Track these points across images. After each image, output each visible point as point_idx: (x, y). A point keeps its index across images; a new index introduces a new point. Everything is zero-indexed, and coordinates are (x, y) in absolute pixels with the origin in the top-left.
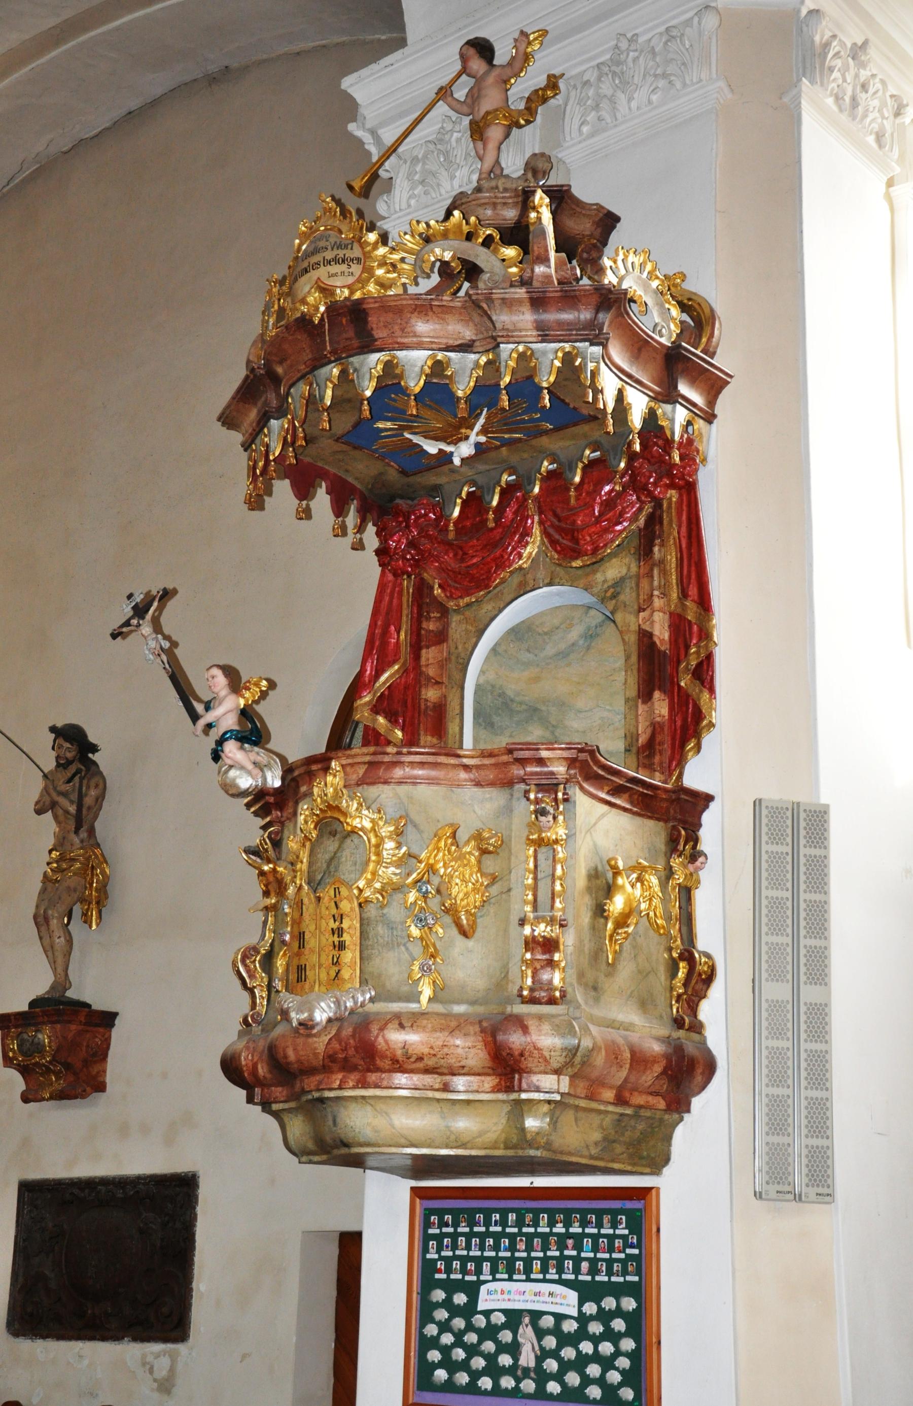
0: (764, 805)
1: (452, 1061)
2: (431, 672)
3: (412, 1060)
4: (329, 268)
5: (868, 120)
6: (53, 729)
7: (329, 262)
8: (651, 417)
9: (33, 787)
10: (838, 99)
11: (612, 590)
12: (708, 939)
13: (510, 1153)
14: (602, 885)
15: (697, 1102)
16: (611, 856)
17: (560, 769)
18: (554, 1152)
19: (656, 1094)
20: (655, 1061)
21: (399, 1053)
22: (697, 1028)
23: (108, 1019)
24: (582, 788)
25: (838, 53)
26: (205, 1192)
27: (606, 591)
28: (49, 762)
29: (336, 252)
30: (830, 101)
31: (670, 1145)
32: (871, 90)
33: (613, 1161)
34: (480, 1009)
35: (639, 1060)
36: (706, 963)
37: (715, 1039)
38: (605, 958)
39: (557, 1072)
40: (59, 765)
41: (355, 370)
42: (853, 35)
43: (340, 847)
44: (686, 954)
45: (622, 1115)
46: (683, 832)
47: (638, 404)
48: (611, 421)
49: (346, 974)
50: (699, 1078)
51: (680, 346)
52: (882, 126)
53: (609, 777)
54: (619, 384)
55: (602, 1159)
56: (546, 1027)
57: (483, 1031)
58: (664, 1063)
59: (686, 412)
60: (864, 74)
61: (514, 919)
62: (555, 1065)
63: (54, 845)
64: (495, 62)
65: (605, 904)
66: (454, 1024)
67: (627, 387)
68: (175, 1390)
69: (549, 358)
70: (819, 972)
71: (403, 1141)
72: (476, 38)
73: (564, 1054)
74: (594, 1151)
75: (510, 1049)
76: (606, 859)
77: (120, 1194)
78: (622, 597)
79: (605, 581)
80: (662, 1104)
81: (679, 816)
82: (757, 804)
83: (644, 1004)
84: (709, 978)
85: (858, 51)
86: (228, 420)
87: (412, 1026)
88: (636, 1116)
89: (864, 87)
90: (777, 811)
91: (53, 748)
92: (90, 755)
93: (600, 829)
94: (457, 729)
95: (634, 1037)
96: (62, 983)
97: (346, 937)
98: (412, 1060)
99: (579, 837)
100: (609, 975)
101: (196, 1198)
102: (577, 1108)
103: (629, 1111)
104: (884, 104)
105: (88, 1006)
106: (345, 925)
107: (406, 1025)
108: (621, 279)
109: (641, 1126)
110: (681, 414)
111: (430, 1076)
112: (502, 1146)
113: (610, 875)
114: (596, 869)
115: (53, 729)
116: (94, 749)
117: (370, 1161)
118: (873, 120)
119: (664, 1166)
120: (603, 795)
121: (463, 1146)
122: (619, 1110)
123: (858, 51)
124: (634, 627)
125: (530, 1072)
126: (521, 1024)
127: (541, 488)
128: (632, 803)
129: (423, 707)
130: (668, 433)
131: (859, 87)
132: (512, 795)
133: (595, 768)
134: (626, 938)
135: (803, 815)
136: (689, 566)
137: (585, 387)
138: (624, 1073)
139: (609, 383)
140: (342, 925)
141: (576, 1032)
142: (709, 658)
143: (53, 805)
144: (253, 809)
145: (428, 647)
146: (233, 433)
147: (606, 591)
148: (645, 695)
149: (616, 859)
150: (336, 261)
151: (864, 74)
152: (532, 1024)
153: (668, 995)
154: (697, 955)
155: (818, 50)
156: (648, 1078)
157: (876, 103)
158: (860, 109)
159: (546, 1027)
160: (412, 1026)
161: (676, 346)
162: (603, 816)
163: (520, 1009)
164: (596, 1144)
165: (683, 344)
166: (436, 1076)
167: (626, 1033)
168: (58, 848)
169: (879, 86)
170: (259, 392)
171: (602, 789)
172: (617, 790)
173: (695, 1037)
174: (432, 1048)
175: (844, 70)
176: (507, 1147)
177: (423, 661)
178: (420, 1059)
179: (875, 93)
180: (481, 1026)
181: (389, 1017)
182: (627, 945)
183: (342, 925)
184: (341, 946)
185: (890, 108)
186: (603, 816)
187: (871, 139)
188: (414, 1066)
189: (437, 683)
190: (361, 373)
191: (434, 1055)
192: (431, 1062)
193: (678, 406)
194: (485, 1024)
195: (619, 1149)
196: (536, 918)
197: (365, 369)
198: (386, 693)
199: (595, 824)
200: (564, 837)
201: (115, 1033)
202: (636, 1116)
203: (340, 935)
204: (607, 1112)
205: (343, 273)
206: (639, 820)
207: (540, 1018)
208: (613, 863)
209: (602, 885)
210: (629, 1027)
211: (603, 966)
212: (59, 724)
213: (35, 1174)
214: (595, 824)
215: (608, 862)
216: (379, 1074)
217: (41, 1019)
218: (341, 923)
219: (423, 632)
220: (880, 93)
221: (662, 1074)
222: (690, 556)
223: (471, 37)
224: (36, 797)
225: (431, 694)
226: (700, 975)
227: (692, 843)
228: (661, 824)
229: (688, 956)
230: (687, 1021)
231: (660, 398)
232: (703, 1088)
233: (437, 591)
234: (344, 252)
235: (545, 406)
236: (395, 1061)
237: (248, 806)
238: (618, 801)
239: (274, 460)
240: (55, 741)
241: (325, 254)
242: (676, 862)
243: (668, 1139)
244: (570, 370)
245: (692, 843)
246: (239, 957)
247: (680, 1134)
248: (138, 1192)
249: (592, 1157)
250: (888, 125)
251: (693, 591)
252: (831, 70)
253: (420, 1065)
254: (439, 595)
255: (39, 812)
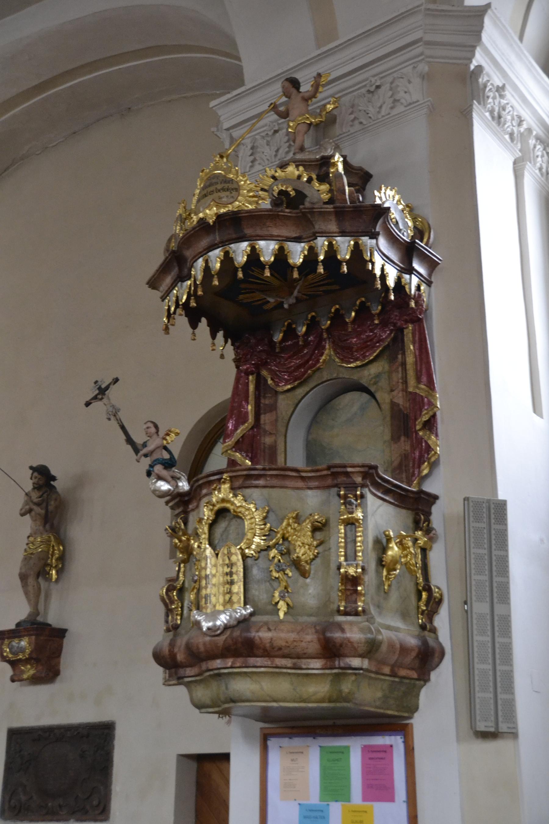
0: (470, 501)
1: (299, 650)
2: (267, 427)
3: (276, 649)
4: (219, 194)
5: (506, 126)
6: (31, 468)
7: (219, 191)
8: (399, 281)
9: (19, 501)
10: (492, 112)
11: (374, 380)
12: (439, 579)
13: (332, 705)
14: (381, 546)
15: (433, 675)
16: (385, 529)
17: (359, 479)
18: (356, 704)
19: (412, 669)
20: (412, 650)
21: (268, 645)
22: (434, 630)
23: (61, 633)
24: (370, 490)
25: (491, 89)
26: (119, 732)
27: (370, 381)
28: (29, 486)
29: (223, 185)
30: (487, 114)
31: (418, 700)
32: (507, 111)
33: (388, 709)
34: (313, 619)
35: (404, 650)
36: (438, 592)
37: (444, 636)
38: (383, 589)
39: (362, 656)
40: (34, 488)
41: (234, 252)
42: (498, 81)
43: (229, 524)
44: (427, 587)
45: (393, 682)
46: (422, 517)
47: (392, 274)
48: (379, 282)
49: (235, 598)
50: (436, 660)
51: (415, 242)
52: (512, 130)
53: (383, 484)
54: (382, 262)
55: (382, 708)
56: (355, 629)
57: (317, 632)
58: (417, 651)
59: (417, 279)
60: (504, 102)
61: (333, 566)
62: (360, 651)
63: (31, 534)
64: (301, 90)
65: (383, 557)
66: (299, 628)
67: (386, 264)
68: (115, 377)
69: (344, 247)
70: (505, 597)
71: (268, 698)
72: (291, 77)
73: (367, 645)
74: (378, 703)
75: (335, 642)
76: (382, 531)
77: (69, 734)
78: (380, 384)
79: (370, 375)
80: (415, 675)
81: (418, 506)
82: (466, 499)
83: (404, 615)
84: (439, 602)
85: (500, 90)
86: (153, 284)
87: (275, 629)
88: (401, 682)
89: (504, 109)
90: (478, 504)
91: (31, 479)
92: (52, 483)
93: (378, 514)
94: (283, 460)
95: (401, 635)
96: (36, 613)
97: (235, 577)
98: (276, 649)
99: (369, 517)
100: (386, 599)
101: (114, 735)
102: (371, 678)
103: (397, 680)
104: (513, 119)
105: (50, 625)
106: (234, 570)
107: (271, 628)
108: (384, 203)
109: (403, 689)
110: (415, 280)
111: (285, 659)
112: (327, 701)
113: (384, 541)
114: (377, 538)
115: (31, 468)
116: (54, 478)
117: (234, 711)
118: (508, 127)
119: (415, 712)
120: (380, 494)
121: (304, 701)
122: (392, 679)
123: (500, 90)
124: (388, 400)
125: (346, 656)
126: (340, 627)
127: (394, 296)
128: (394, 500)
129: (262, 447)
130: (407, 290)
131: (501, 109)
132: (330, 493)
133: (377, 478)
134: (394, 578)
135: (492, 506)
136: (421, 365)
137: (366, 261)
138: (395, 657)
139: (378, 261)
140: (232, 570)
141: (373, 632)
142: (434, 416)
143: (30, 511)
144: (170, 504)
145: (265, 414)
146: (155, 291)
147: (370, 381)
148: (395, 438)
149: (389, 531)
150: (223, 190)
151: (504, 102)
152: (346, 627)
153: (416, 611)
154: (433, 587)
155: (481, 86)
156: (408, 659)
157: (509, 117)
158: (502, 119)
159: (355, 629)
160: (275, 629)
161: (413, 243)
162: (380, 506)
163: (340, 618)
164: (379, 699)
165: (417, 241)
166: (289, 659)
167: (396, 633)
168: (33, 535)
169: (510, 109)
170: (176, 263)
171: (378, 490)
172: (387, 492)
173: (432, 635)
174: (287, 642)
175: (494, 98)
176: (330, 701)
177: (262, 422)
178: (280, 649)
179: (509, 112)
180: (316, 629)
181: (261, 624)
182: (394, 583)
183: (232, 570)
184: (232, 583)
185: (516, 121)
186: (380, 506)
187: (507, 137)
188: (277, 653)
189: (271, 434)
190: (237, 253)
191: (289, 647)
192: (286, 651)
193: (413, 276)
194: (318, 628)
195: (392, 702)
196: (348, 565)
197: (240, 251)
198: (241, 440)
199: (376, 511)
200: (361, 518)
201: (65, 641)
202: (401, 682)
203: (231, 576)
204: (385, 680)
205: (227, 196)
206: (398, 509)
207: (351, 623)
208: (387, 533)
209: (381, 546)
210: (397, 629)
211: (382, 593)
212: (35, 465)
213: (17, 724)
214: (376, 511)
215: (384, 533)
216: (254, 658)
217: (23, 633)
218: (232, 568)
219: (262, 405)
220: (511, 113)
221: (415, 657)
222: (421, 359)
223: (288, 77)
224: (20, 506)
225: (268, 440)
226: (435, 599)
227: (427, 523)
228: (410, 512)
229: (428, 589)
230: (428, 628)
231: (403, 271)
232: (438, 665)
233: (270, 382)
234: (228, 185)
235: (344, 272)
236: (265, 650)
237: (167, 503)
238: (387, 498)
239: (182, 305)
240: (32, 474)
241: (216, 186)
242: (419, 533)
243: (418, 696)
244: (357, 251)
245: (427, 523)
246: (164, 591)
247: (423, 693)
248: (79, 733)
249: (377, 707)
250: (515, 129)
251: (424, 379)
252: (488, 97)
253: (280, 653)
254: (271, 384)
255: (22, 515)
